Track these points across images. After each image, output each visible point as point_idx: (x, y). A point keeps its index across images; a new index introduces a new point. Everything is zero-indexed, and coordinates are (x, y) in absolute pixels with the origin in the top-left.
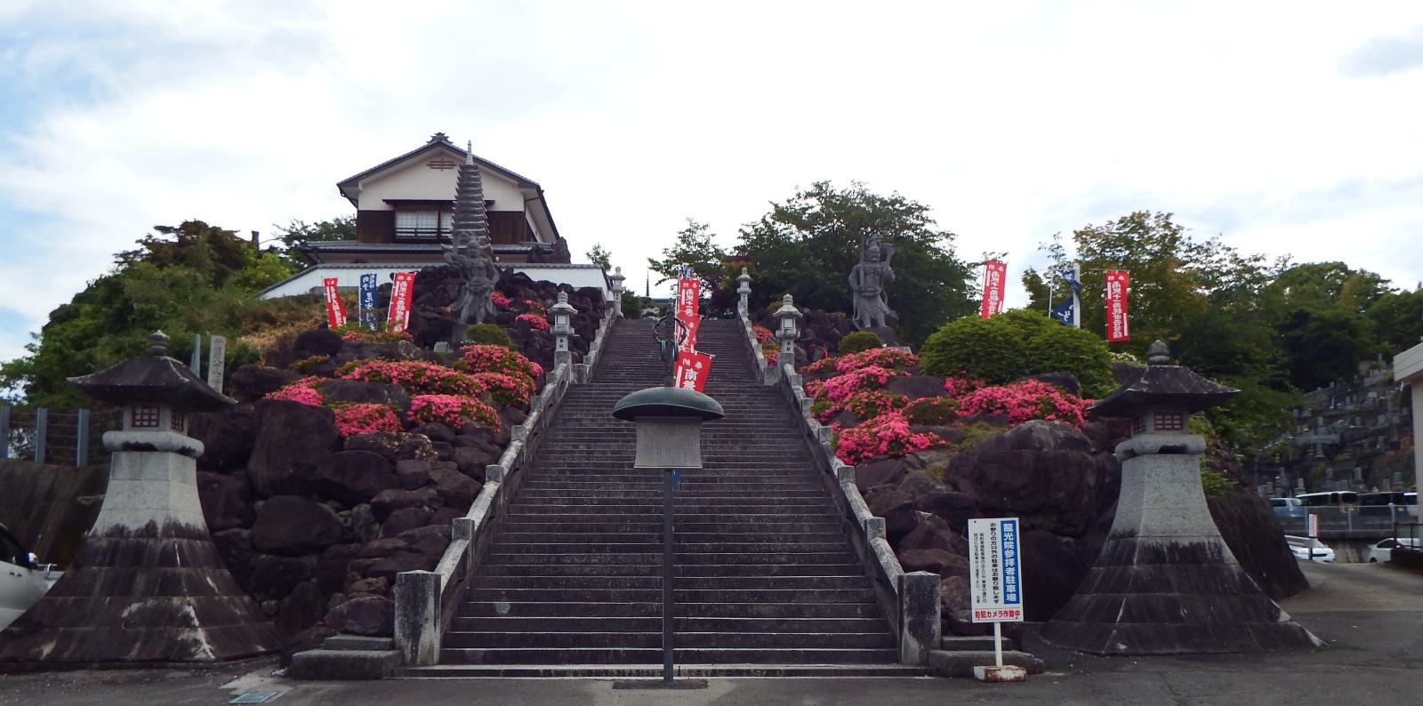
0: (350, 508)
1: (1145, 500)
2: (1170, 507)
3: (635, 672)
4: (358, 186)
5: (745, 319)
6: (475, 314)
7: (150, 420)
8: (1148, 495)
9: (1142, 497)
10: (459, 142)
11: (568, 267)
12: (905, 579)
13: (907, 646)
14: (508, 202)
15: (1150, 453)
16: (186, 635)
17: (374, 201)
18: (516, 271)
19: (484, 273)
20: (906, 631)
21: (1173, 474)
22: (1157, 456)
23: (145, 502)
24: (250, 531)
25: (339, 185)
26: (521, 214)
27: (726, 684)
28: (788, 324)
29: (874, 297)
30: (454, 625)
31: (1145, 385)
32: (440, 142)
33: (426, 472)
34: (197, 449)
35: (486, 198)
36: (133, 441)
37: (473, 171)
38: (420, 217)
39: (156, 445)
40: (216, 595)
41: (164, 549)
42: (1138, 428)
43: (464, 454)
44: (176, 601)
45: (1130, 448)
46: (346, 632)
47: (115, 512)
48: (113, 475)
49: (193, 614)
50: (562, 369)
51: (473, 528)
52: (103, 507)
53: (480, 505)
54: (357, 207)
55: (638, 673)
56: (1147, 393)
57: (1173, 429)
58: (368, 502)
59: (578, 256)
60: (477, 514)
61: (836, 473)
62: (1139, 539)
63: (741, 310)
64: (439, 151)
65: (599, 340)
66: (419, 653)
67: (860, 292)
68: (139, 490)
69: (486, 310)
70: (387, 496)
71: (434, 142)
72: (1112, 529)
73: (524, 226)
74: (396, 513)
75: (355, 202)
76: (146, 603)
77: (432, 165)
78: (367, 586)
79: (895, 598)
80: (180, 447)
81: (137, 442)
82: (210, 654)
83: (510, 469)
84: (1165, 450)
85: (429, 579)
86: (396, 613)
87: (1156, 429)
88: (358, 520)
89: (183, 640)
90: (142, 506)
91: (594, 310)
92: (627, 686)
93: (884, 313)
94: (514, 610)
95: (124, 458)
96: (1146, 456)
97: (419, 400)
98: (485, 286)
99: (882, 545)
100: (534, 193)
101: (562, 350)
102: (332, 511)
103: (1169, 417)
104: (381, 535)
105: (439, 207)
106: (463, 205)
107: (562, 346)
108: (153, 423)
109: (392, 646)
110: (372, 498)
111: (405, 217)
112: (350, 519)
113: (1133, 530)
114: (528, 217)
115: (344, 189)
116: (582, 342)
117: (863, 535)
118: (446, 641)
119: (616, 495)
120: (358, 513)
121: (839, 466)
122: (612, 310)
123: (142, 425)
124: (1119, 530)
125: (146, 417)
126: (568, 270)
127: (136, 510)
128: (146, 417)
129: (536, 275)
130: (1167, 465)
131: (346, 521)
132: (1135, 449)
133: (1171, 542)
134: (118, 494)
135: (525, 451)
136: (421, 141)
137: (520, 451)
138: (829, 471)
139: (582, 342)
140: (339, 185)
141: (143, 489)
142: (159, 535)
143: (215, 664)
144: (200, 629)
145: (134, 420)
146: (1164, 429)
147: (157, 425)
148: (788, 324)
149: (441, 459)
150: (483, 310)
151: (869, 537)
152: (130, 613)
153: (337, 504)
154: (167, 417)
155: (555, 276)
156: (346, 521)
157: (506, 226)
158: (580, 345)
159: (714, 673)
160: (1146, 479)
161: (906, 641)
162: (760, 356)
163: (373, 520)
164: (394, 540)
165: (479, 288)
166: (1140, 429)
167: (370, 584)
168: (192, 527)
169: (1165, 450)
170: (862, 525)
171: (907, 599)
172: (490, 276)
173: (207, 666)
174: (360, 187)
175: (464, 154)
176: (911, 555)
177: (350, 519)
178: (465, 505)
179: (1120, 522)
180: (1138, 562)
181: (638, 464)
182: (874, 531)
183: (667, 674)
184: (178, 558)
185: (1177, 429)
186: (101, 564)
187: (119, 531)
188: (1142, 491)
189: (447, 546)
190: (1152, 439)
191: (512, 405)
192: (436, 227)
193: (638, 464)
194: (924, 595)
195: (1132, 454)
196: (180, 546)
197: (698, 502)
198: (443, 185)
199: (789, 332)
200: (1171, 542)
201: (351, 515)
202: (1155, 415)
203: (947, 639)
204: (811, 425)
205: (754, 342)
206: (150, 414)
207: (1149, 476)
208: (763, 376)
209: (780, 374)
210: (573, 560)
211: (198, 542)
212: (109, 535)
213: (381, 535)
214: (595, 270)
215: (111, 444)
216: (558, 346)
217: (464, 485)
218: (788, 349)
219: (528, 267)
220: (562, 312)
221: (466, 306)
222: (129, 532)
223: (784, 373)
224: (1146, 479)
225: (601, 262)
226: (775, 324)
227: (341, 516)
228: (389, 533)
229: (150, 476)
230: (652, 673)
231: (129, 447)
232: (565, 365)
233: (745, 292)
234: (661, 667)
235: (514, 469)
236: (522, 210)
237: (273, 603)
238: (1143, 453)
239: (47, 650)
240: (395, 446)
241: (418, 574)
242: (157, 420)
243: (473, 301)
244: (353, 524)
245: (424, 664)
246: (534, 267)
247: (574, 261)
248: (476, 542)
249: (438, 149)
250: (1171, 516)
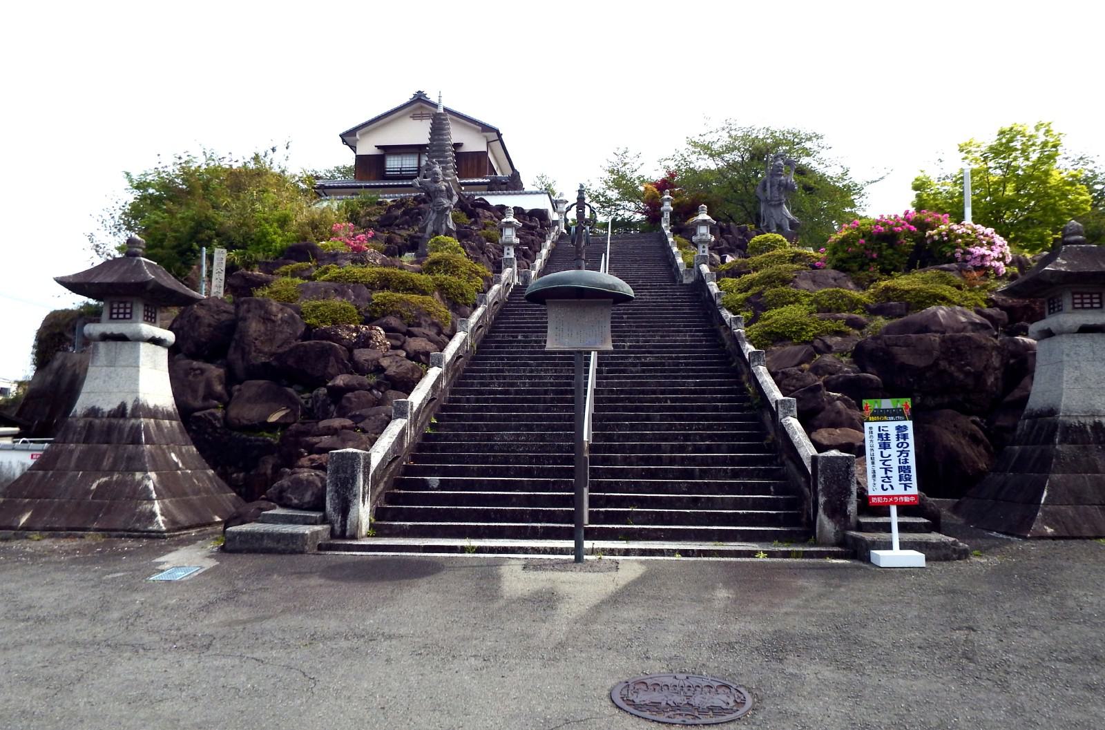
0: (311, 392)
1: (1065, 379)
2: (1092, 386)
3: (549, 550)
5: (667, 232)
7: (125, 313)
8: (1068, 374)
9: (1061, 377)
10: (433, 98)
11: (521, 194)
12: (820, 459)
13: (822, 526)
14: (473, 143)
15: (1069, 332)
16: (146, 507)
17: (368, 147)
18: (476, 198)
20: (821, 511)
21: (1094, 353)
22: (1076, 335)
23: (118, 387)
26: (485, 154)
27: (636, 566)
28: (703, 230)
29: (780, 204)
30: (391, 498)
31: (1062, 265)
32: (420, 98)
33: (378, 359)
34: (168, 339)
35: (454, 141)
36: (108, 332)
37: (440, 120)
38: (404, 158)
39: (128, 335)
40: (180, 469)
41: (132, 427)
42: (1054, 308)
43: (416, 344)
44: (138, 476)
45: (1046, 328)
46: (284, 506)
47: (92, 395)
48: (92, 363)
49: (151, 487)
50: (509, 274)
51: (412, 409)
52: (83, 391)
53: (422, 389)
54: (355, 152)
55: (553, 551)
56: (1066, 272)
57: (1092, 308)
58: (325, 386)
59: (527, 182)
60: (417, 397)
61: (747, 357)
62: (1060, 418)
63: (664, 225)
64: (419, 105)
65: (544, 252)
66: (348, 527)
67: (767, 201)
68: (113, 375)
69: (447, 225)
70: (340, 380)
72: (1028, 407)
73: (484, 166)
74: (349, 395)
75: (353, 148)
76: (112, 478)
77: (414, 117)
78: (309, 463)
79: (811, 480)
80: (150, 337)
81: (112, 333)
82: (162, 525)
83: (453, 356)
84: (1085, 329)
85: (359, 457)
86: (328, 489)
87: (1075, 308)
88: (317, 402)
89: (140, 512)
90: (115, 390)
91: (542, 227)
92: (539, 566)
93: (789, 219)
94: (443, 485)
95: (102, 346)
96: (1064, 335)
97: (378, 296)
99: (793, 424)
100: (493, 136)
101: (509, 257)
102: (295, 394)
103: (1088, 296)
104: (335, 414)
105: (417, 150)
106: (433, 148)
107: (510, 253)
108: (128, 316)
109: (324, 520)
111: (392, 159)
112: (310, 401)
113: (1052, 409)
114: (490, 155)
115: (346, 138)
116: (530, 252)
117: (775, 415)
118: (378, 514)
119: (546, 379)
120: (317, 396)
121: (749, 351)
122: (557, 228)
123: (118, 318)
124: (1036, 409)
125: (122, 311)
126: (520, 196)
127: (110, 393)
128: (122, 311)
129: (494, 200)
130: (1087, 344)
131: (307, 402)
132: (1052, 328)
133: (1095, 422)
134: (96, 378)
135: (469, 341)
136: (406, 98)
137: (464, 340)
138: (741, 354)
139: (530, 252)
140: (901, 549)
141: (117, 375)
142: (128, 416)
143: (166, 534)
144: (156, 502)
145: (111, 314)
146: (1083, 308)
147: (131, 318)
148: (703, 230)
149: (393, 347)
150: (444, 226)
151: (780, 416)
152: (98, 486)
153: (300, 388)
154: (140, 311)
155: (510, 201)
156: (307, 402)
157: (471, 163)
158: (526, 254)
159: (627, 552)
160: (1065, 358)
161: (821, 520)
162: (680, 260)
163: (329, 402)
164: (342, 420)
166: (1055, 308)
167: (312, 461)
168: (160, 409)
169: (1085, 329)
170: (774, 405)
171: (822, 480)
172: (450, 197)
173: (159, 535)
174: (357, 136)
175: (436, 106)
176: (823, 435)
177: (310, 401)
178: (407, 386)
179: (1037, 400)
180: (1061, 442)
181: (550, 345)
182: (785, 411)
183: (578, 552)
184: (143, 437)
185: (1096, 308)
186: (77, 442)
187: (93, 412)
188: (1061, 370)
189: (388, 423)
190: (1071, 319)
191: (459, 304)
193: (550, 345)
194: (839, 475)
195: (1048, 334)
196: (147, 426)
197: (620, 384)
198: (417, 132)
199: (704, 237)
200: (1095, 422)
201: (311, 397)
202: (1074, 293)
203: (863, 520)
204: (724, 315)
205: (675, 249)
206: (125, 308)
207: (1068, 355)
208: (682, 277)
209: (696, 273)
210: (503, 437)
211: (167, 422)
212: (86, 415)
213: (335, 414)
214: (543, 195)
215: (90, 335)
216: (505, 253)
217: (413, 370)
218: (703, 252)
219: (488, 194)
220: (509, 224)
221: (431, 222)
222: (103, 413)
223: (700, 272)
224: (1065, 358)
225: (549, 191)
226: (692, 231)
227: (302, 398)
228: (342, 414)
229: (123, 363)
230: (561, 551)
231: (105, 337)
232: (511, 269)
233: (667, 210)
234: (570, 544)
235: (457, 357)
236: (484, 149)
237: (242, 475)
238: (1061, 333)
239: (23, 520)
241: (348, 453)
242: (131, 313)
243: (437, 218)
244: (313, 406)
245: (354, 537)
246: (493, 194)
248: (416, 419)
249: (418, 104)
250: (1093, 395)
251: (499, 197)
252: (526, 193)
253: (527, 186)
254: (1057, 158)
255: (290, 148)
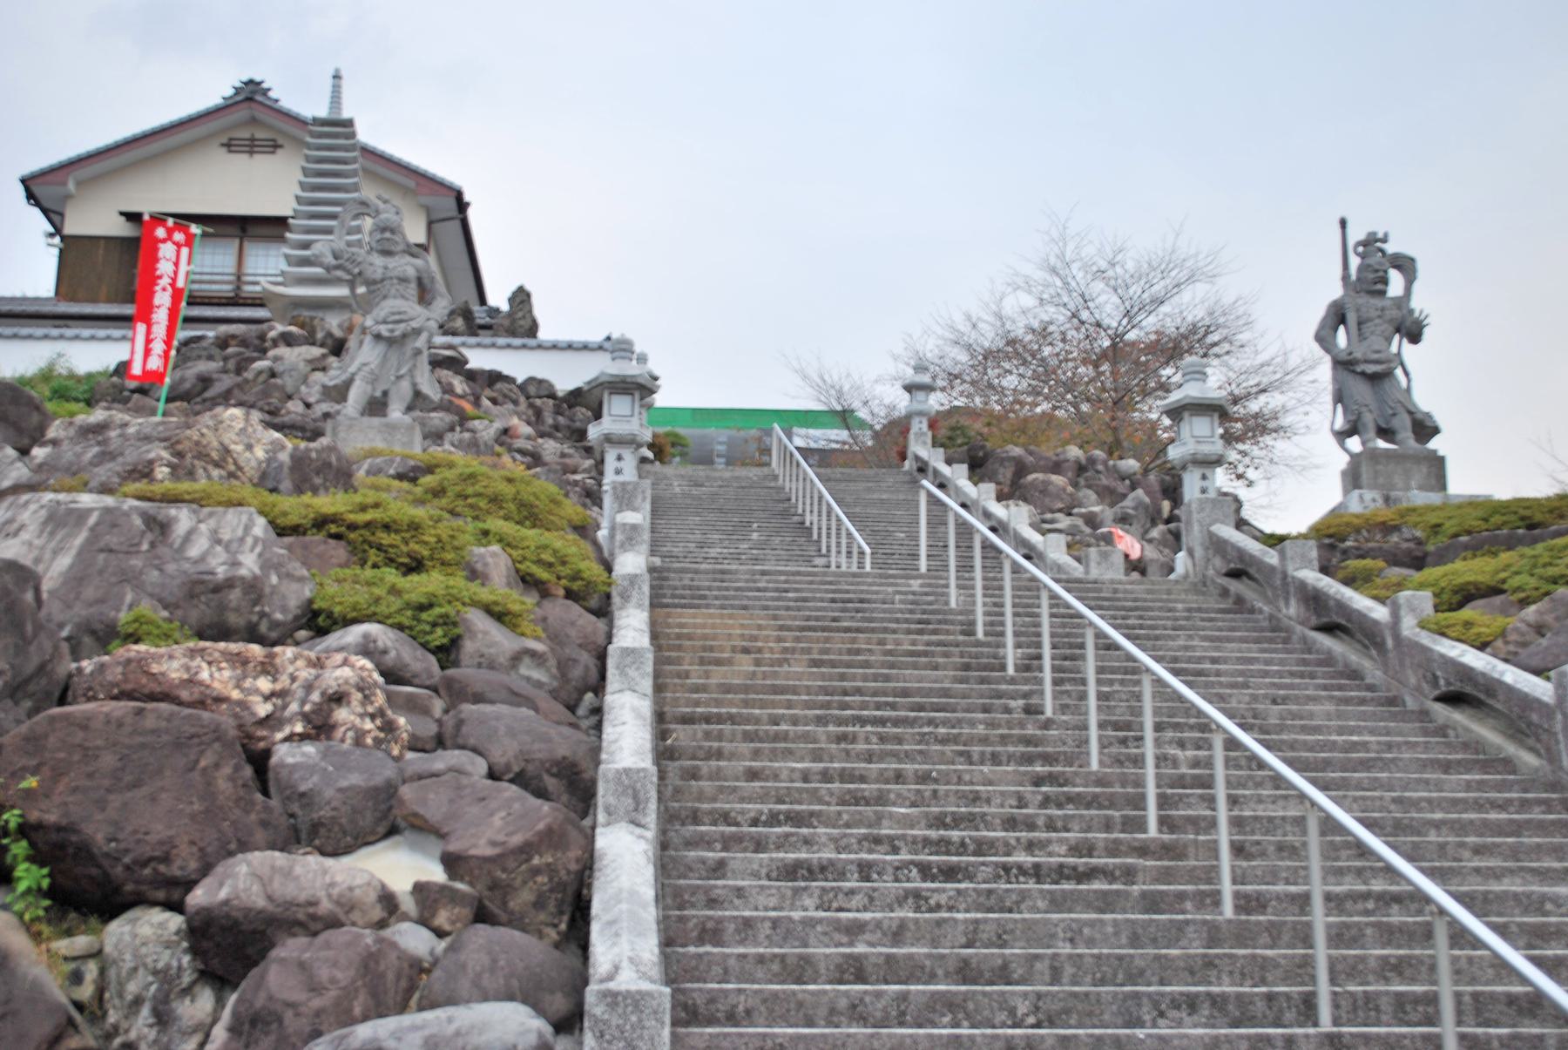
4: (65, 184)
6: (385, 393)
17: (98, 218)
19: (412, 289)
24: (315, 816)
25: (24, 181)
32: (251, 94)
58: (176, 907)
64: (249, 119)
69: (414, 385)
70: (243, 881)
71: (239, 98)
98: (414, 324)
110: (189, 885)
112: (91, 970)
115: (36, 190)
155: (516, 364)
165: (400, 329)
174: (71, 186)
177: (91, 970)
192: (232, 270)
201: (97, 954)
240: (257, 691)
247: (544, 334)
249: (242, 113)
251: (492, 353)
252: (540, 347)
253: (125, 357)
254: (1036, 325)
255: (331, 72)
